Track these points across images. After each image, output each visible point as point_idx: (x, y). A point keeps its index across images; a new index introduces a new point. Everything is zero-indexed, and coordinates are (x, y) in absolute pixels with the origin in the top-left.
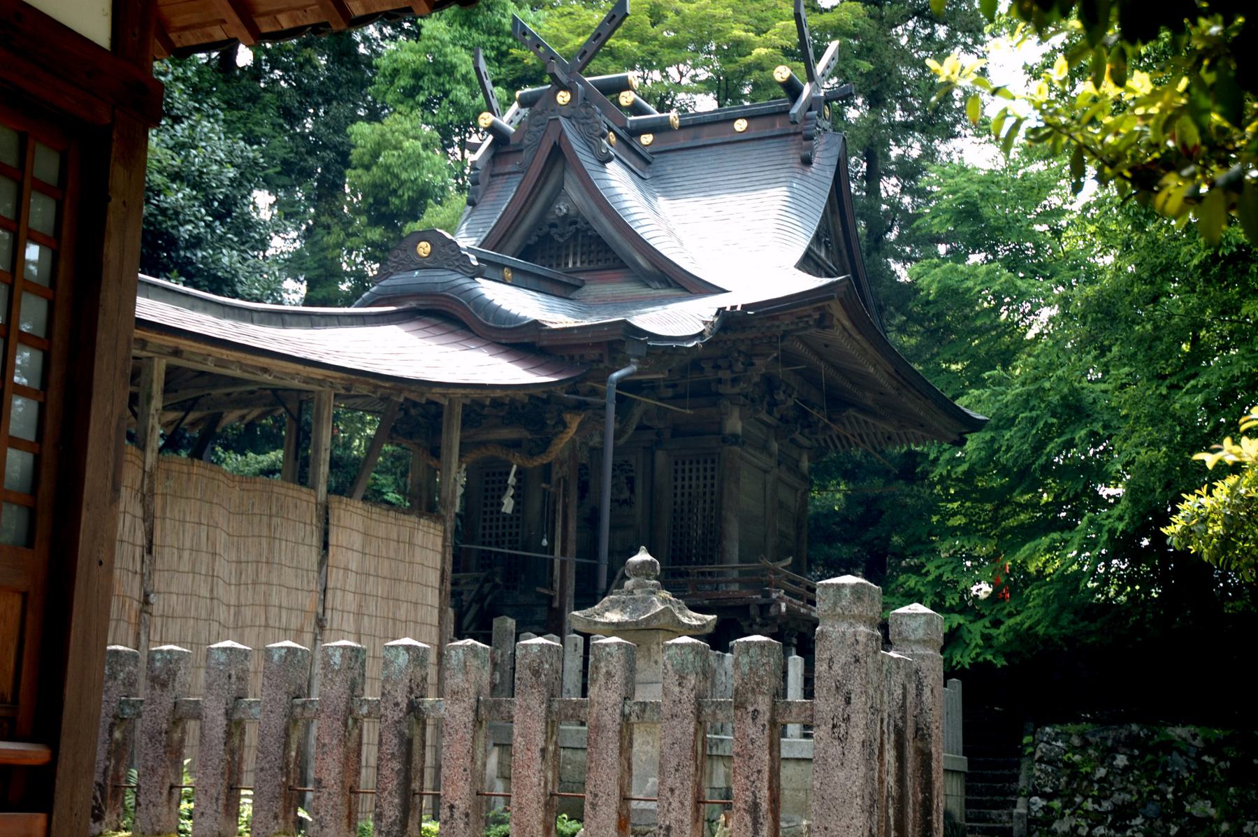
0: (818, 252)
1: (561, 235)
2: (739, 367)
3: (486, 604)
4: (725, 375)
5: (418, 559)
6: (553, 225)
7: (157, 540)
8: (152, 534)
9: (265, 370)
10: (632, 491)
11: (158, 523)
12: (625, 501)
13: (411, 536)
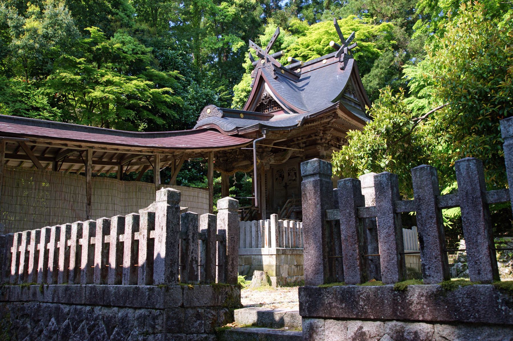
0: (350, 96)
1: (266, 102)
2: (321, 135)
3: (253, 215)
4: (318, 138)
5: (200, 201)
6: (263, 100)
7: (92, 200)
8: (90, 199)
9: (117, 149)
10: (296, 176)
11: (92, 197)
12: (294, 180)
13: (198, 194)
